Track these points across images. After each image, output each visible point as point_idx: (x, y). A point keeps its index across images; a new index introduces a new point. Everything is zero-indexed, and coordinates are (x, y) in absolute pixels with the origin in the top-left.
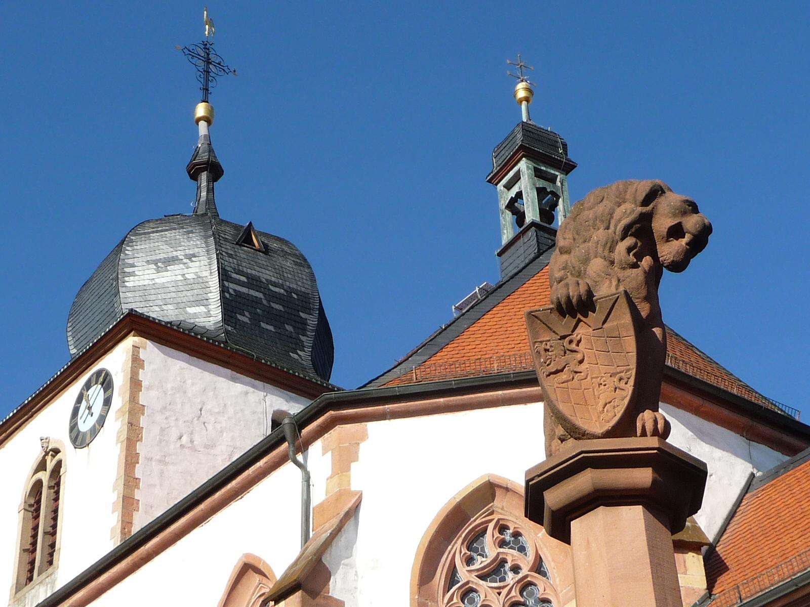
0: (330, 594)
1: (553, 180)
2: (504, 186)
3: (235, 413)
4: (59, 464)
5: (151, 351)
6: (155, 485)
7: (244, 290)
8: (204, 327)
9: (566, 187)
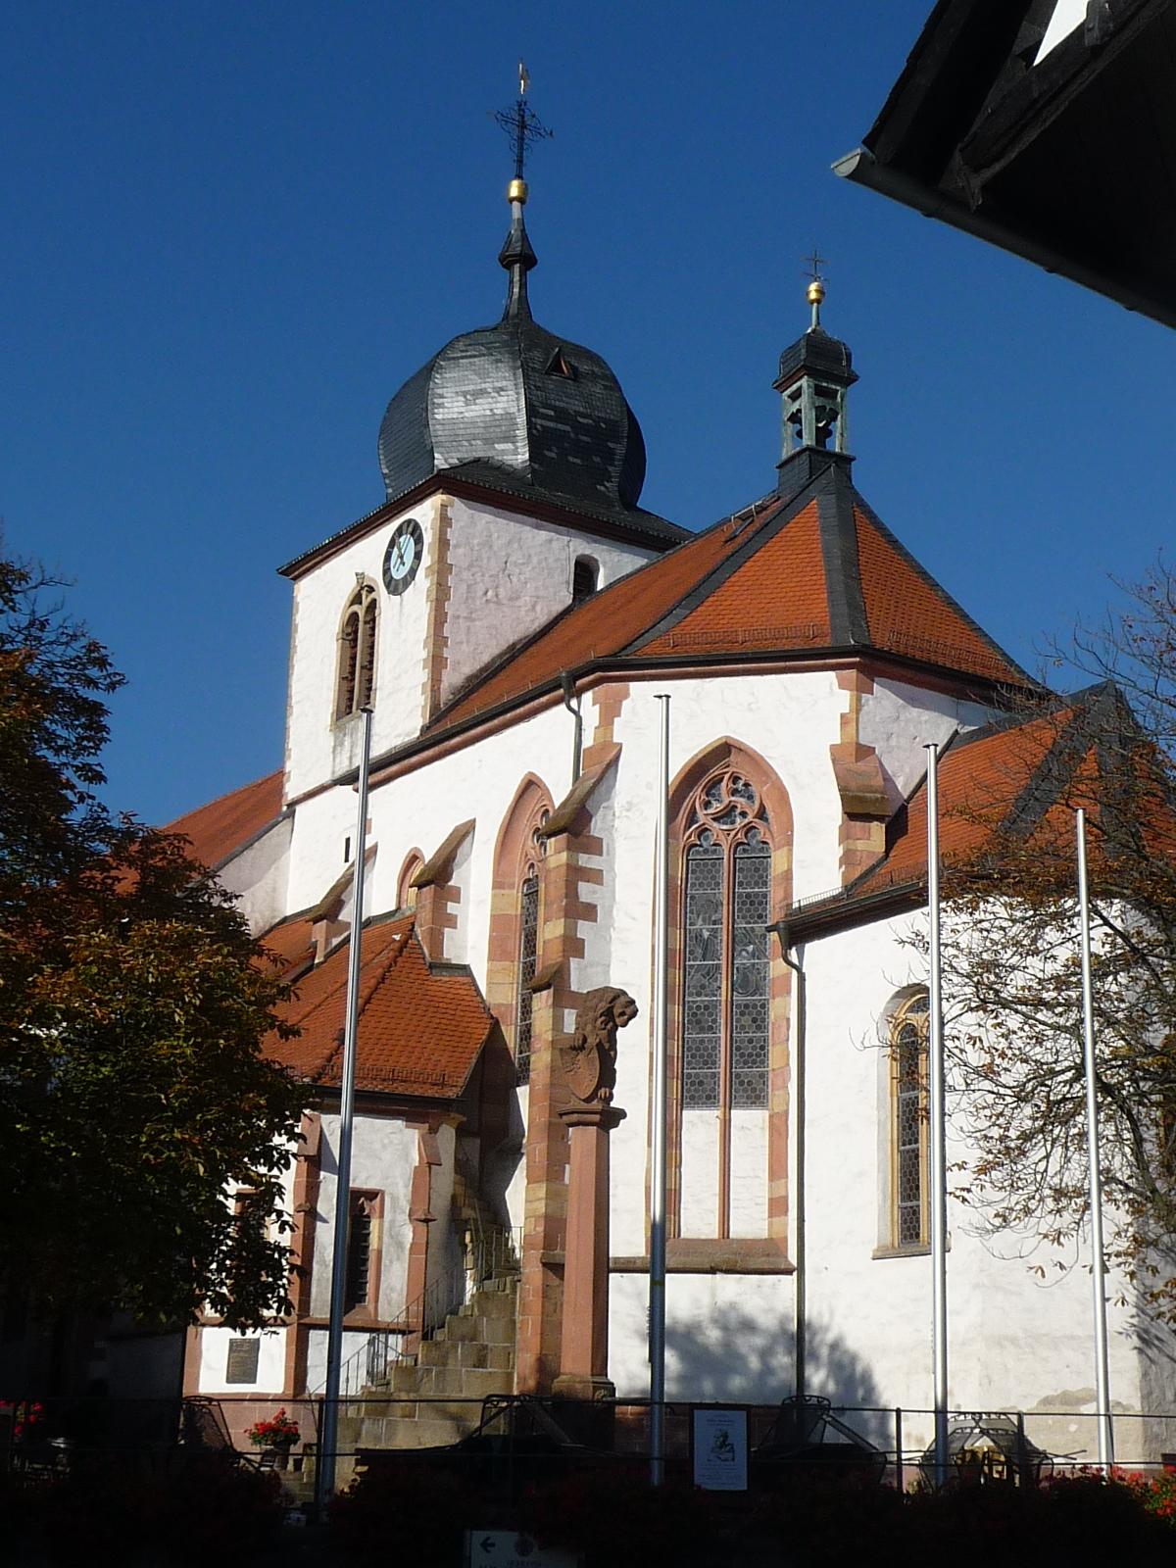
0: (591, 833)
1: (833, 394)
2: (789, 397)
3: (539, 563)
4: (373, 605)
6: (462, 643)
7: (551, 424)
8: (511, 466)
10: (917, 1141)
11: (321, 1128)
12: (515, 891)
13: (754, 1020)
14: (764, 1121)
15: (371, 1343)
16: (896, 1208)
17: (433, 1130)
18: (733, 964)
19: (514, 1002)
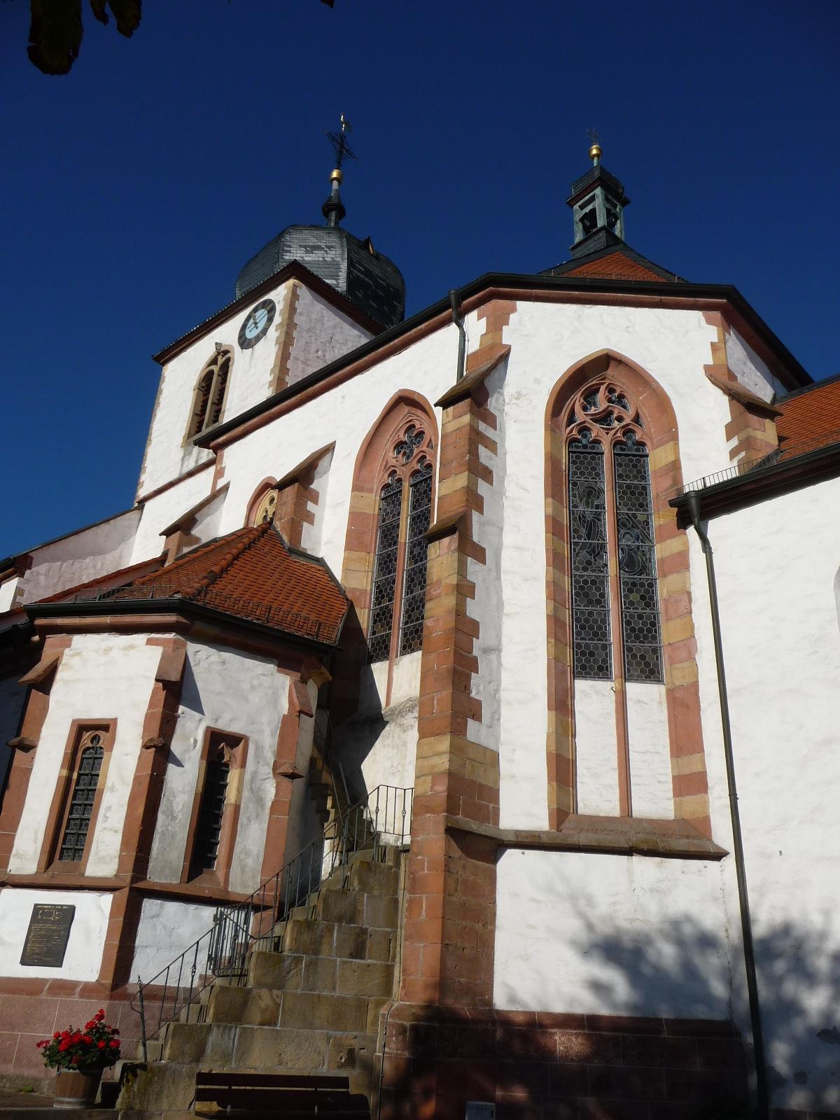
1: (615, 207)
5: (304, 291)
7: (362, 276)
9: (622, 214)
11: (186, 657)
12: (373, 495)
13: (643, 598)
14: (660, 695)
15: (219, 920)
18: (618, 545)
19: (368, 589)
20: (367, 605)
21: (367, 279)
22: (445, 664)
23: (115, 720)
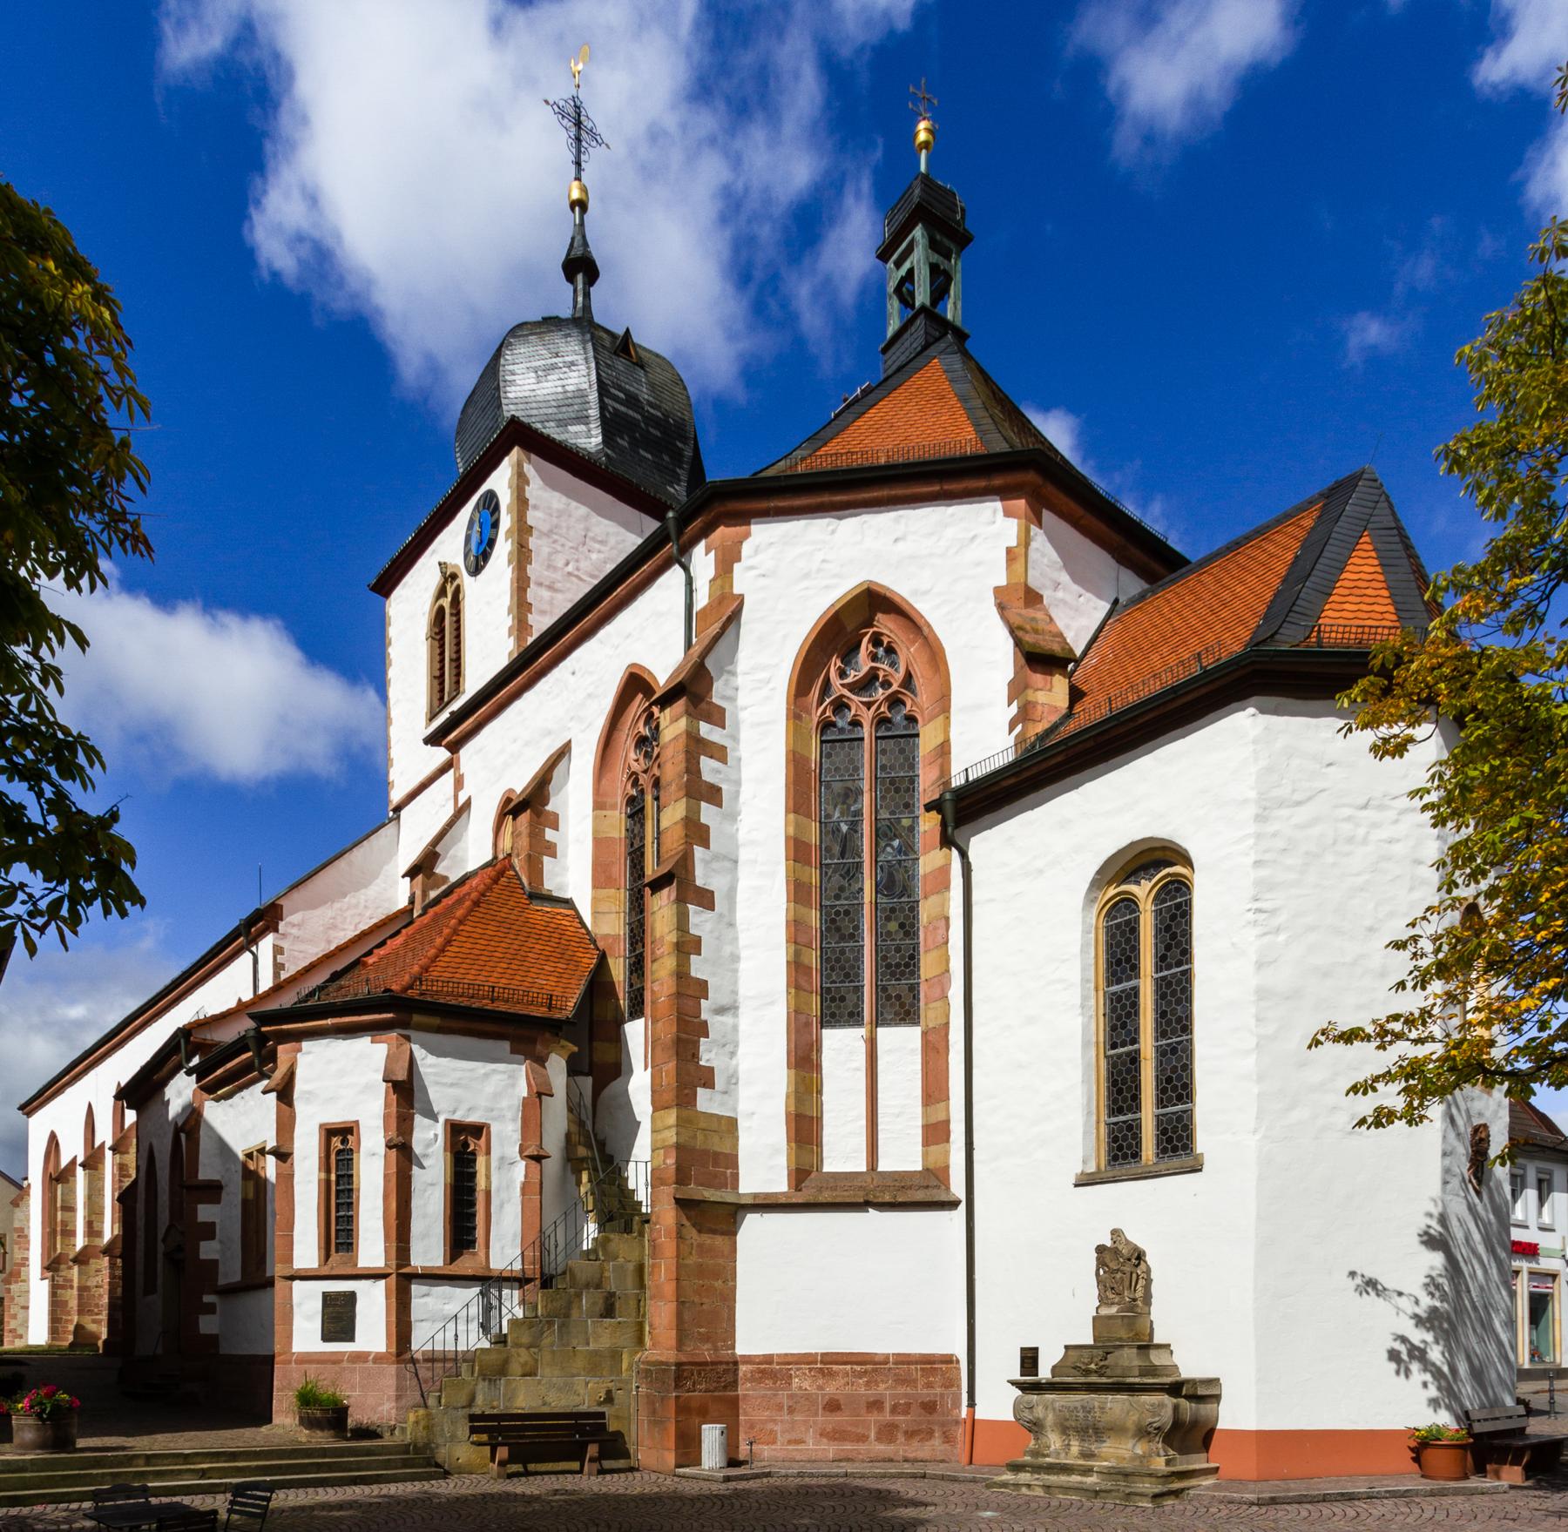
4: (457, 591)
7: (623, 409)
8: (585, 449)
10: (1135, 1041)
13: (902, 926)
16: (1102, 1125)
17: (541, 1061)
18: (876, 862)
20: (622, 953)
21: (631, 413)
22: (668, 1030)
23: (357, 1122)
